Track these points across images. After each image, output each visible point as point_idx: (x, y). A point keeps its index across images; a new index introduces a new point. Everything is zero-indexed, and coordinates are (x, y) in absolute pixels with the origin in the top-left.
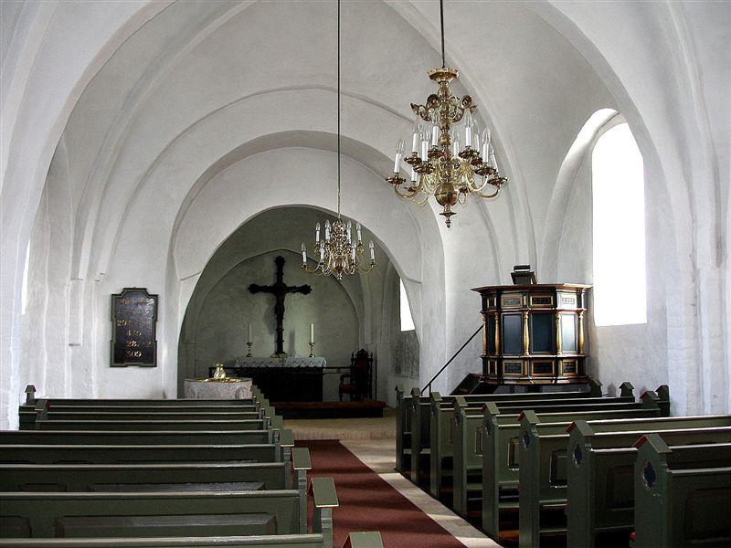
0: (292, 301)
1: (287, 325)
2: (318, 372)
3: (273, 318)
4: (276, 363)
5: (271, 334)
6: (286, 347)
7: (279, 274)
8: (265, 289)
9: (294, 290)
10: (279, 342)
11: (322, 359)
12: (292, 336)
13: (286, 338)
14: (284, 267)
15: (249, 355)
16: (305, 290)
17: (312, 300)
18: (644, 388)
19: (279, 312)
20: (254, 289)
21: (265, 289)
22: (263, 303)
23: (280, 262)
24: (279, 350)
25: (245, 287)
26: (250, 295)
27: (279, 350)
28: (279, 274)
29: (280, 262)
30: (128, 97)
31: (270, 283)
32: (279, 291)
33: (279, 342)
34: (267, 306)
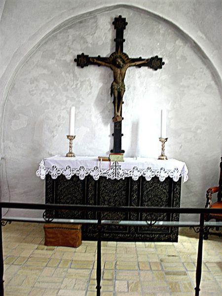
0: (136, 80)
1: (127, 110)
2: (172, 186)
3: (110, 101)
4: (104, 170)
5: (106, 123)
6: (125, 144)
7: (119, 41)
8: (98, 61)
9: (140, 63)
10: (117, 135)
11: (180, 165)
12: (135, 127)
13: (126, 129)
14: (125, 32)
15: (70, 154)
16: (155, 63)
17: (164, 77)
18: (109, 136)
19: (117, 95)
20: (83, 61)
21: (98, 61)
22: (95, 79)
23: (120, 25)
24: (117, 149)
25: (70, 58)
26: (77, 70)
27: (117, 149)
28: (119, 41)
29: (120, 25)
30: (81, 22)
31: (106, 52)
32: (116, 63)
33: (117, 135)
34: (101, 85)
